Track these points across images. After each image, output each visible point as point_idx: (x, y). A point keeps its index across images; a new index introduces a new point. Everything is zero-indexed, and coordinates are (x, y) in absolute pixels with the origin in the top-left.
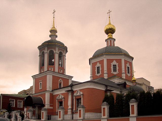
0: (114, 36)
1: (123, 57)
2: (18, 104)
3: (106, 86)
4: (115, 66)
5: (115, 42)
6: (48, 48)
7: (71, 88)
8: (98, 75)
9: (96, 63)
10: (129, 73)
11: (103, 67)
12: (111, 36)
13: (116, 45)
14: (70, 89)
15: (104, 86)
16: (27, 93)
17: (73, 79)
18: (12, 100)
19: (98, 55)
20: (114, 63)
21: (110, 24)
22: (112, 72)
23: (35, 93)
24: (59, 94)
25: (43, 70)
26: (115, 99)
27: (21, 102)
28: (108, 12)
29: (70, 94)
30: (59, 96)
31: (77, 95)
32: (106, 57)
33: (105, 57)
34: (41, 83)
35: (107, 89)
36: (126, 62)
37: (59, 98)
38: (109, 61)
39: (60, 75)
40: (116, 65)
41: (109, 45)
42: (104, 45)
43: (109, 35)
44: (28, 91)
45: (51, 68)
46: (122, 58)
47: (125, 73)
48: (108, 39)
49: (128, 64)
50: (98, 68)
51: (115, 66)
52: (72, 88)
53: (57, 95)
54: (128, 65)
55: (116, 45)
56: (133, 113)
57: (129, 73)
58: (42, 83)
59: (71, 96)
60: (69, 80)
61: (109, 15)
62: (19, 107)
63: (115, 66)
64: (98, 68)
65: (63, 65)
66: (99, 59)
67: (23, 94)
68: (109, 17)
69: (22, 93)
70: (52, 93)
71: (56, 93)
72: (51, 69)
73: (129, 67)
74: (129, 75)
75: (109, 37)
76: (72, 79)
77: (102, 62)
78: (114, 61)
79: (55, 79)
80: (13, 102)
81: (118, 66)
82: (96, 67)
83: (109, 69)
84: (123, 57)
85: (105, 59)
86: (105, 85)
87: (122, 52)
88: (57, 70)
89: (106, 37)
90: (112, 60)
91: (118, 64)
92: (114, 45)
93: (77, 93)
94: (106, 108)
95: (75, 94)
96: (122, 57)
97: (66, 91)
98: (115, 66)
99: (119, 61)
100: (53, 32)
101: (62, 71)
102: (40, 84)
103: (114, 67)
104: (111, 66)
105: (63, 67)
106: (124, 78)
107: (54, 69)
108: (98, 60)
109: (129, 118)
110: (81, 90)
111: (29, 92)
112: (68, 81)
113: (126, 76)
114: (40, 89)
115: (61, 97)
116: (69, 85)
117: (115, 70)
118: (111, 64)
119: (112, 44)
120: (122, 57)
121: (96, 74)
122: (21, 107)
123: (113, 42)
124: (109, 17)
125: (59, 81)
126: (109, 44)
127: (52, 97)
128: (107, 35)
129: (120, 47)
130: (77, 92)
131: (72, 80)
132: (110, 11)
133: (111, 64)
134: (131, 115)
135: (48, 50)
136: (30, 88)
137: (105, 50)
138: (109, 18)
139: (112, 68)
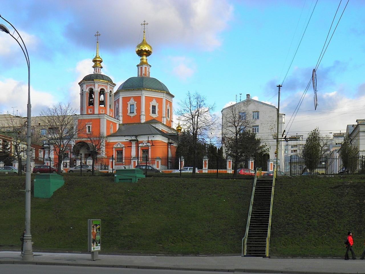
0: (149, 60)
8: (132, 115)
9: (130, 98)
20: (154, 103)
22: (129, 114)
24: (118, 142)
26: (217, 149)
28: (143, 23)
34: (89, 127)
39: (111, 119)
53: (115, 143)
54: (168, 106)
59: (135, 146)
61: (144, 29)
63: (154, 107)
66: (134, 95)
74: (169, 119)
77: (138, 99)
78: (154, 101)
82: (129, 104)
83: (147, 110)
89: (137, 60)
90: (128, 99)
99: (159, 100)
101: (104, 111)
112: (116, 125)
118: (150, 103)
121: (129, 114)
133: (150, 103)
135: (98, 88)
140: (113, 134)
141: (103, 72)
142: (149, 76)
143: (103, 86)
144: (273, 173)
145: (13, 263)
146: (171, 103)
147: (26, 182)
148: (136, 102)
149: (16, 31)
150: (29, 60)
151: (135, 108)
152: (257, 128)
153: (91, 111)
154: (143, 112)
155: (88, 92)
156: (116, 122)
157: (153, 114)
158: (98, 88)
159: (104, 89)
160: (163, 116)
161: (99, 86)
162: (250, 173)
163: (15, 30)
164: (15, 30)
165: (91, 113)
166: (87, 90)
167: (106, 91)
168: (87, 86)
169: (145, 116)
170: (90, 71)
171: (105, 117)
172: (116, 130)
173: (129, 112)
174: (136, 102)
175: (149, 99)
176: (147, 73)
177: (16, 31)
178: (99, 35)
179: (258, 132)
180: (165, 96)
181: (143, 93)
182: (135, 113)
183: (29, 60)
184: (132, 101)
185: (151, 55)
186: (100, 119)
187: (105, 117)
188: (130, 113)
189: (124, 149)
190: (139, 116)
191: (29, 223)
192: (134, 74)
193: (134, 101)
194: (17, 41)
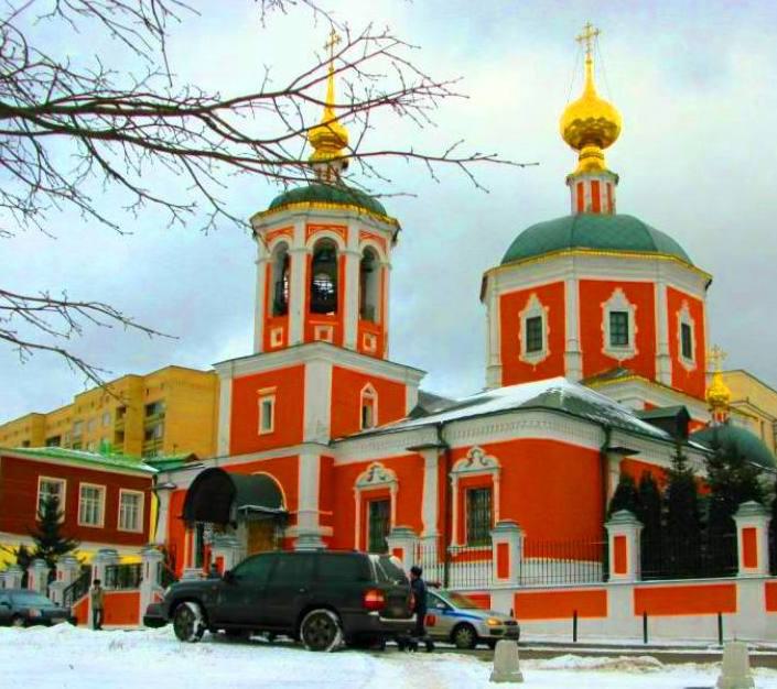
0: (611, 157)
2: (82, 506)
3: (607, 430)
4: (619, 318)
5: (618, 191)
7: (440, 437)
10: (687, 353)
11: (557, 318)
12: (591, 160)
13: (620, 210)
15: (596, 430)
16: (50, 435)
17: (426, 386)
18: (129, 496)
19: (532, 247)
21: (589, 96)
27: (135, 503)
30: (372, 473)
31: (471, 468)
32: (573, 271)
33: (571, 268)
34: (268, 405)
36: (675, 299)
37: (370, 480)
38: (593, 293)
41: (588, 209)
42: (558, 205)
43: (584, 150)
44: (59, 423)
47: (673, 354)
48: (581, 174)
49: (682, 312)
50: (534, 323)
51: (621, 320)
52: (443, 432)
54: (684, 316)
55: (620, 210)
56: (751, 561)
57: (687, 353)
58: (272, 399)
62: (87, 520)
63: (619, 318)
64: (534, 323)
67: (25, 437)
68: (589, 62)
69: (16, 433)
70: (329, 453)
71: (351, 453)
72: (325, 327)
73: (691, 324)
75: (585, 161)
76: (422, 382)
78: (534, 300)
79: (345, 382)
80: (93, 500)
82: (524, 316)
85: (570, 272)
87: (658, 246)
89: (571, 161)
90: (606, 289)
91: (635, 307)
92: (611, 205)
93: (471, 461)
94: (625, 530)
95: (460, 467)
97: (410, 449)
98: (621, 320)
101: (373, 341)
102: (261, 405)
103: (614, 320)
104: (600, 320)
105: (377, 319)
106: (668, 380)
109: (732, 588)
110: (489, 449)
113: (678, 370)
114: (262, 431)
115: (384, 478)
117: (620, 337)
118: (603, 305)
119: (603, 201)
122: (134, 526)
123: (606, 192)
124: (589, 62)
125: (362, 392)
126: (588, 201)
127: (335, 479)
128: (575, 154)
129: (642, 220)
130: (469, 455)
131: (420, 388)
132: (592, 30)
134: (743, 570)
135: (307, 237)
136: (72, 401)
137: (569, 231)
138: (586, 66)
139: (606, 327)
143: (327, 227)
146: (697, 309)
147: (766, 530)
148: (547, 308)
151: (633, 329)
153: (278, 338)
157: (615, 348)
158: (307, 237)
159: (328, 235)
162: (678, 425)
165: (280, 343)
166: (301, 249)
167: (341, 247)
174: (547, 308)
180: (661, 273)
191: (223, 440)
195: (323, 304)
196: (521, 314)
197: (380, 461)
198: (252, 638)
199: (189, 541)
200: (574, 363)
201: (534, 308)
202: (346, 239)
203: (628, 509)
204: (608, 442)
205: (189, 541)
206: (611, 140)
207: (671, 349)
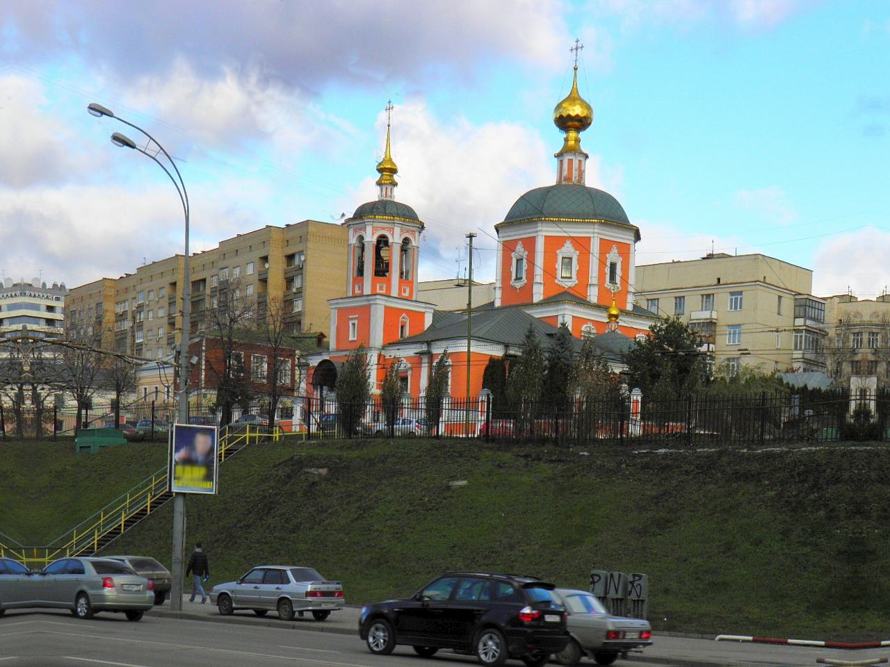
1: (596, 230)
3: (507, 346)
6: (373, 228)
9: (516, 241)
14: (424, 348)
15: (501, 347)
22: (512, 283)
23: (338, 350)
25: (361, 288)
29: (425, 360)
35: (506, 352)
40: (571, 258)
45: (380, 284)
46: (594, 233)
49: (611, 255)
54: (613, 256)
58: (356, 322)
59: (427, 365)
60: (426, 315)
61: (576, 61)
65: (410, 274)
77: (530, 244)
81: (578, 260)
82: (560, 254)
84: (596, 230)
86: (503, 343)
88: (394, 293)
90: (559, 241)
96: (592, 230)
100: (387, 172)
101: (408, 290)
104: (556, 262)
105: (410, 278)
107: (389, 288)
108: (521, 237)
111: (215, 271)
113: (603, 291)
114: (351, 338)
116: (425, 329)
118: (558, 252)
120: (592, 230)
121: (512, 283)
123: (577, 166)
124: (576, 69)
125: (400, 319)
135: (373, 234)
140: (409, 338)
141: (401, 195)
142: (579, 181)
143: (383, 228)
144: (755, 419)
145: (322, 631)
149: (153, 139)
150: (187, 200)
152: (739, 297)
154: (539, 278)
155: (356, 245)
156: (423, 310)
158: (373, 234)
160: (590, 283)
161: (375, 229)
163: (151, 138)
164: (151, 138)
168: (375, 229)
169: (542, 287)
170: (372, 194)
171: (378, 301)
172: (423, 325)
173: (514, 277)
175: (554, 243)
176: (575, 174)
177: (153, 139)
178: (392, 108)
179: (740, 308)
181: (539, 229)
182: (524, 280)
183: (187, 200)
184: (568, 249)
185: (592, 123)
186: (370, 305)
187: (378, 301)
188: (515, 280)
189: (409, 373)
190: (529, 288)
192: (548, 178)
193: (523, 250)
194: (155, 160)
195: (382, 269)
196: (513, 255)
197: (405, 357)
198: (790, 641)
199: (317, 394)
200: (595, 247)
201: (520, 250)
202: (393, 235)
203: (487, 388)
204: (506, 352)
205: (317, 394)
206: (170, 588)
207: (599, 279)
